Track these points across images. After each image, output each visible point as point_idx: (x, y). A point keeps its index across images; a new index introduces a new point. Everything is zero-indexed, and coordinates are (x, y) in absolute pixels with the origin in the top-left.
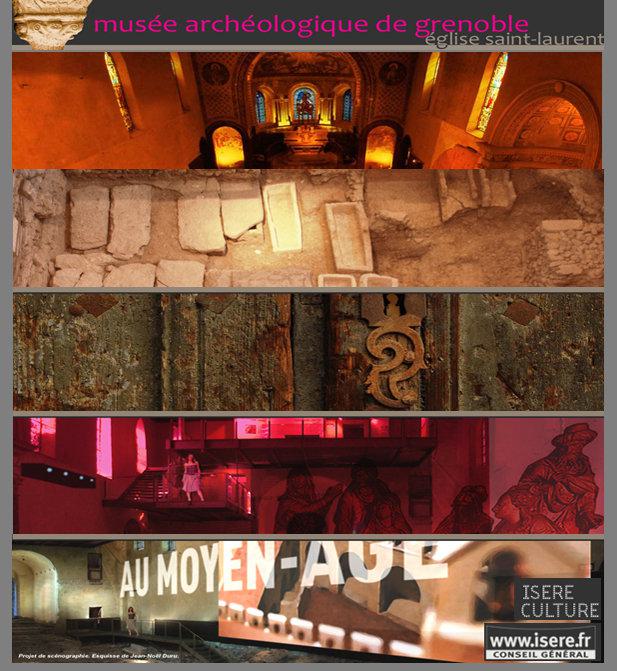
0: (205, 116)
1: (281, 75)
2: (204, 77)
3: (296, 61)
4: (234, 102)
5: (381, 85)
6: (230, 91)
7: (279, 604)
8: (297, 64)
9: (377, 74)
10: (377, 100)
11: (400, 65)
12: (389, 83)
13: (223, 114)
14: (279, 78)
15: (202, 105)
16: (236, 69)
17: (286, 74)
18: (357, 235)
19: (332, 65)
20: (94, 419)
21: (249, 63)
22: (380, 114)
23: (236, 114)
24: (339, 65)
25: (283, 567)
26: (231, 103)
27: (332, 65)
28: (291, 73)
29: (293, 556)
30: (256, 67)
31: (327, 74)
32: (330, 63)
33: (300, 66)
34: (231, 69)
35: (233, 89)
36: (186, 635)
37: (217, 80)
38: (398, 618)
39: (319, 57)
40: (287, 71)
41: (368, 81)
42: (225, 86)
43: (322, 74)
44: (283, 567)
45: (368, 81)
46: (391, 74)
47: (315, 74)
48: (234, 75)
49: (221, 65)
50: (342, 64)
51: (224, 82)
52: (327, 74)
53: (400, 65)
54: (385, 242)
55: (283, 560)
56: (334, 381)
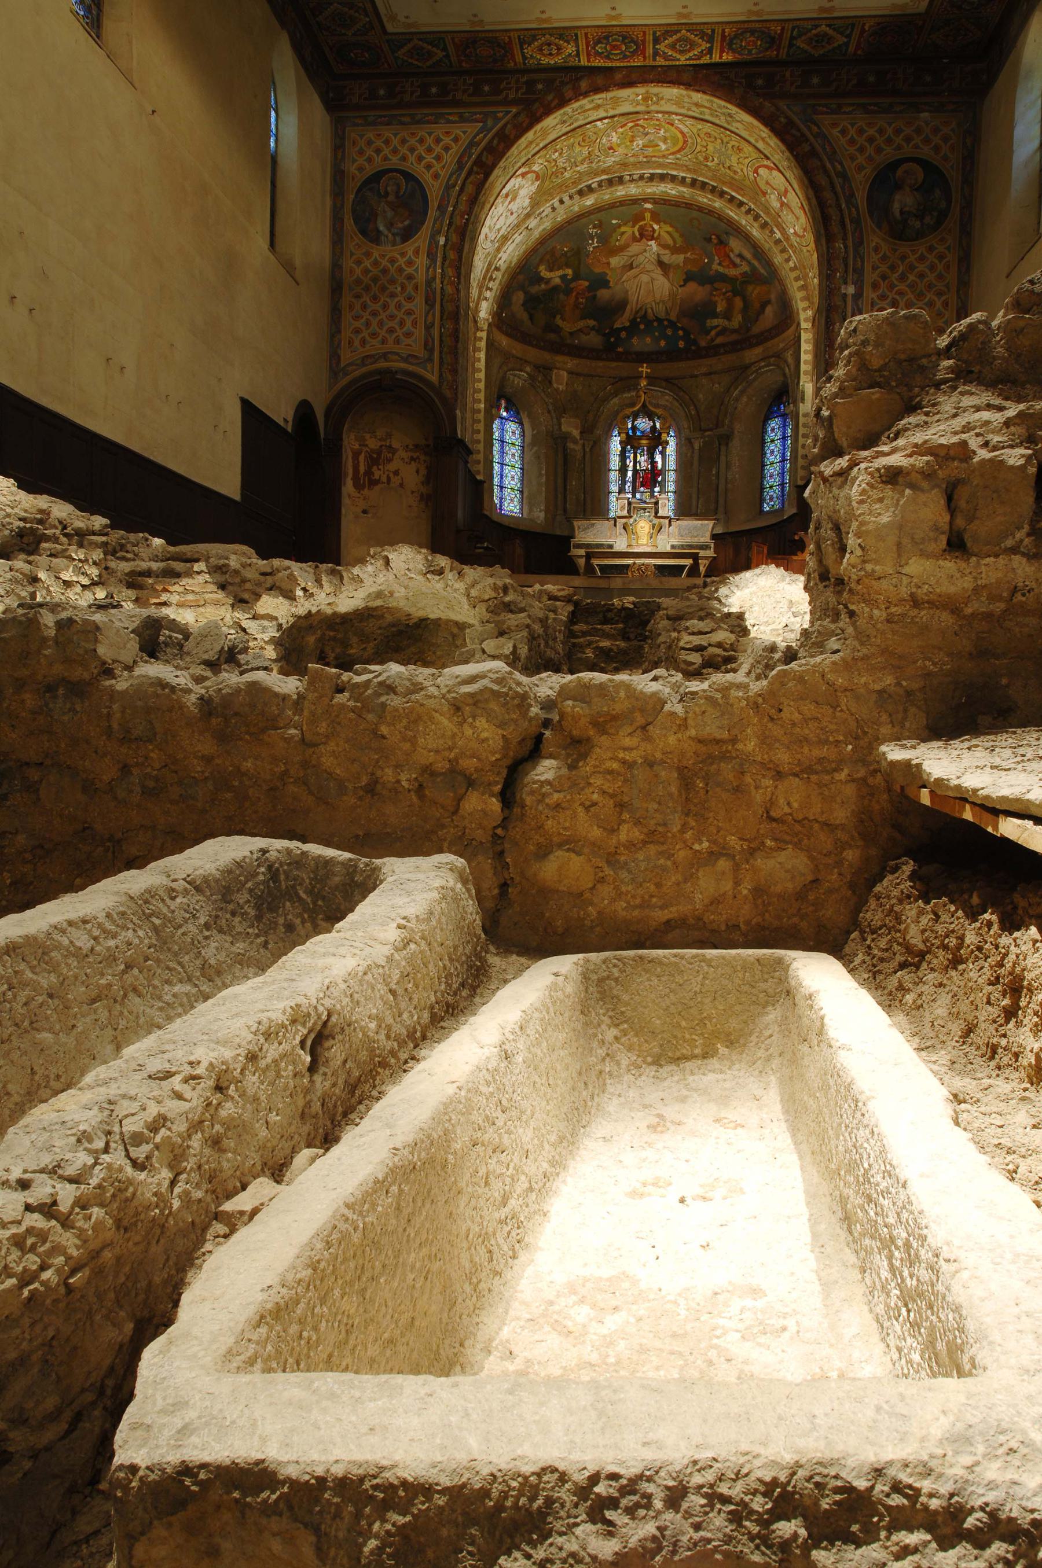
2: (357, 219)
4: (429, 301)
5: (875, 239)
6: (422, 261)
8: (622, 321)
9: (861, 198)
14: (571, 363)
15: (335, 313)
16: (449, 187)
18: (673, 1067)
19: (727, 315)
23: (428, 346)
26: (419, 304)
28: (612, 348)
31: (713, 351)
33: (633, 328)
34: (434, 190)
35: (431, 255)
36: (118, 1388)
37: (390, 225)
38: (811, 1197)
40: (594, 340)
41: (835, 228)
42: (410, 248)
45: (835, 228)
46: (903, 201)
47: (671, 355)
48: (441, 208)
49: (408, 176)
51: (407, 235)
54: (806, 415)
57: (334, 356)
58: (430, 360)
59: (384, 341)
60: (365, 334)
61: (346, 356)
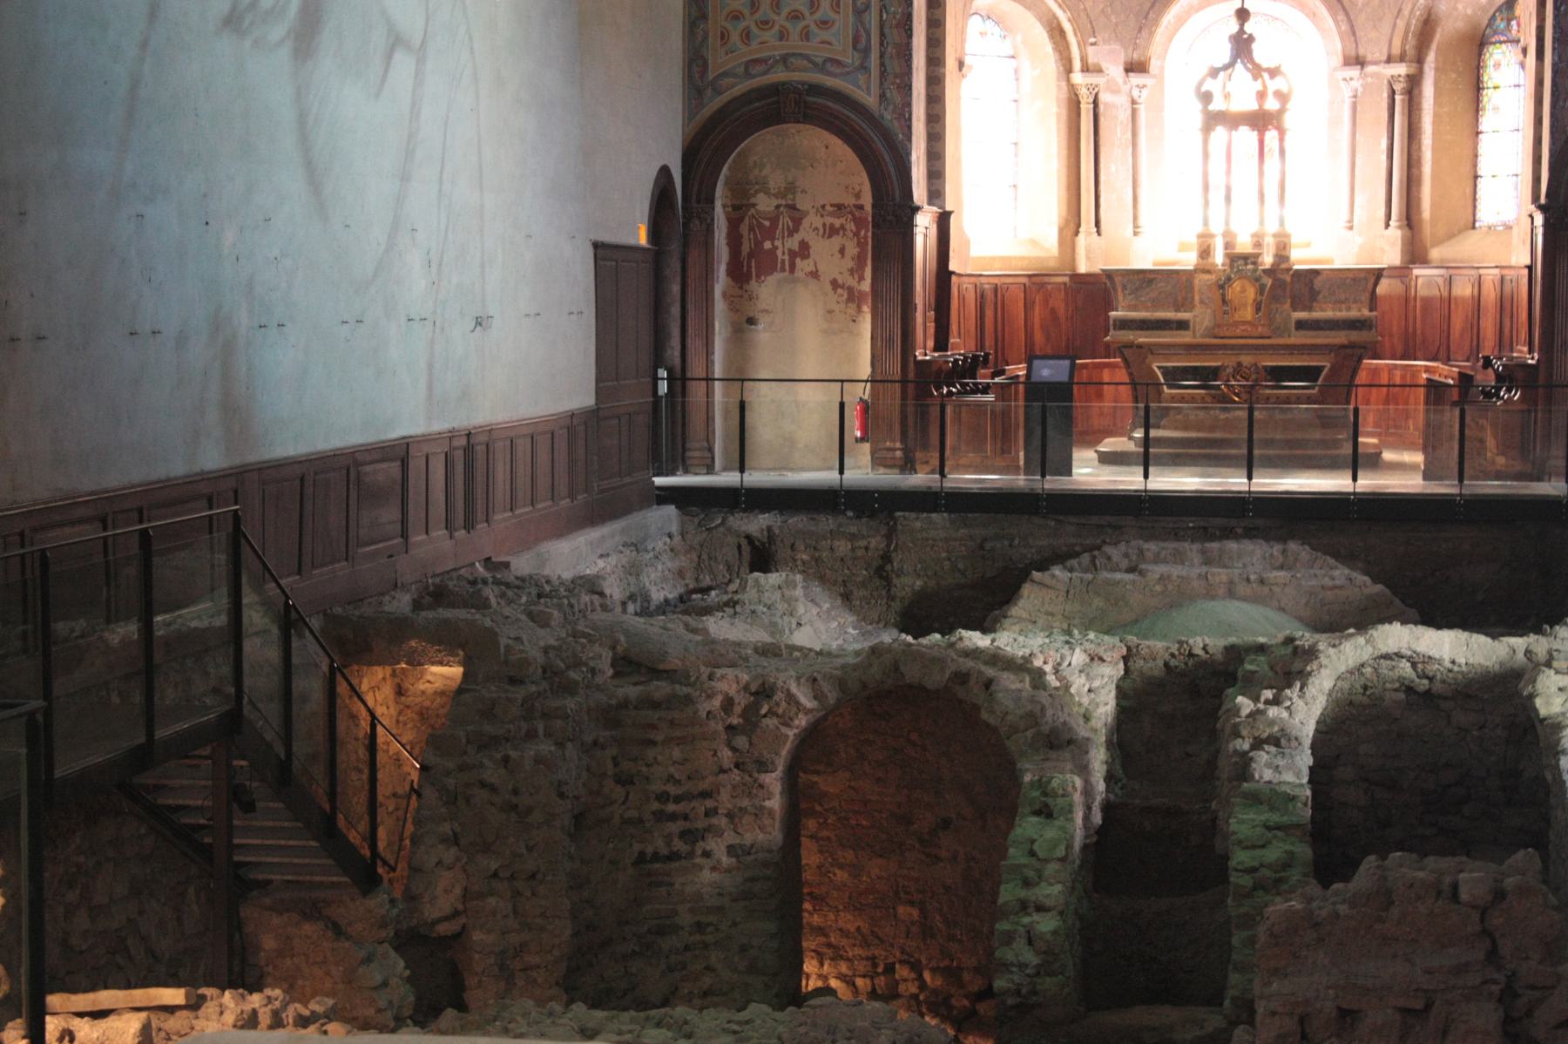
13: (795, 43)
57: (695, 61)
58: (863, 67)
59: (783, 35)
60: (749, 22)
61: (719, 61)
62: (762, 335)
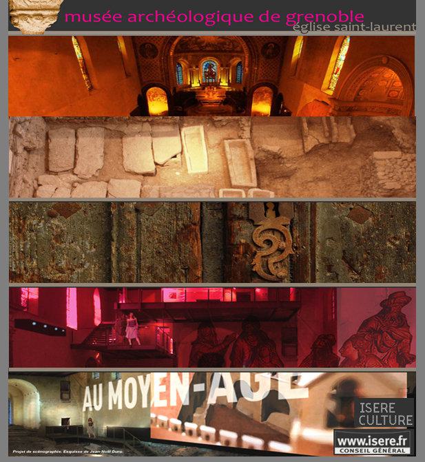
0: (141, 80)
1: (193, 51)
2: (141, 53)
3: (204, 42)
4: (161, 70)
5: (262, 59)
6: (158, 62)
7: (192, 416)
8: (204, 44)
9: (260, 51)
10: (260, 69)
11: (275, 44)
12: (268, 57)
13: (154, 78)
14: (192, 54)
15: (139, 72)
16: (162, 47)
17: (197, 51)
18: (246, 162)
19: (229, 45)
20: (65, 288)
21: (171, 44)
22: (262, 78)
23: (162, 79)
24: (233, 45)
25: (195, 391)
26: (159, 71)
27: (229, 45)
28: (201, 50)
29: (202, 383)
30: (176, 46)
31: (225, 51)
32: (227, 43)
33: (206, 46)
34: (159, 47)
35: (160, 61)
36: (128, 437)
37: (149, 55)
38: (274, 426)
39: (220, 39)
40: (198, 49)
41: (253, 56)
42: (155, 59)
43: (222, 51)
44: (195, 391)
45: (253, 56)
46: (270, 51)
47: (217, 51)
48: (161, 51)
49: (152, 45)
50: (236, 44)
51: (154, 57)
52: (225, 51)
53: (275, 44)
54: (265, 167)
55: (195, 386)
56: (230, 262)
62: (90, 75)
